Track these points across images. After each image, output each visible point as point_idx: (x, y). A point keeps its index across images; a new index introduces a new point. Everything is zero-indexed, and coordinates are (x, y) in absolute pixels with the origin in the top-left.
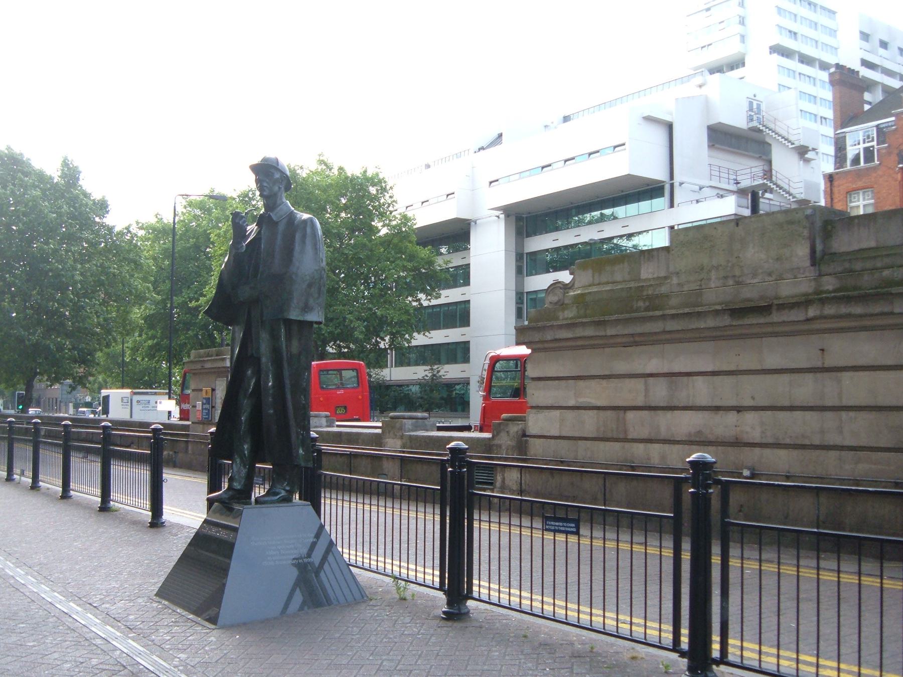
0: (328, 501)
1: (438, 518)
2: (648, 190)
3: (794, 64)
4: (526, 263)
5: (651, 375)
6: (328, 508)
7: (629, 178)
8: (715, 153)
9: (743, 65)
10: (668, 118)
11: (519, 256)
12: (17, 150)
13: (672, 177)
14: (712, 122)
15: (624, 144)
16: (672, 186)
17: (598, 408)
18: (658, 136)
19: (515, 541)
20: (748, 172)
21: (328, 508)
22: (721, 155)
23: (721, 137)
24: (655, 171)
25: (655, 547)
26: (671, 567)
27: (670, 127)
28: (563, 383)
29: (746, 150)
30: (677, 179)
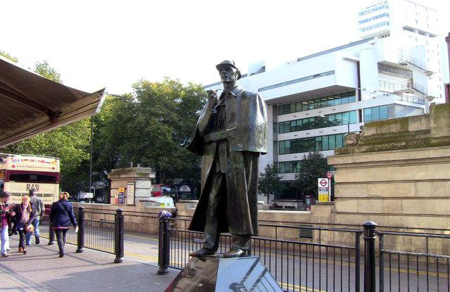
0: (173, 250)
1: (353, 265)
2: (347, 93)
3: (416, 35)
4: (278, 128)
5: (419, 181)
6: (173, 253)
7: (337, 87)
8: (380, 74)
9: (389, 35)
10: (357, 59)
11: (275, 124)
12: (173, 78)
13: (359, 86)
14: (381, 60)
15: (333, 72)
16: (360, 91)
17: (384, 198)
18: (353, 67)
19: (177, 260)
20: (399, 82)
21: (173, 253)
22: (385, 76)
23: (384, 67)
24: (350, 83)
25: (434, 272)
26: (354, 278)
27: (358, 63)
28: (359, 186)
29: (394, 73)
30: (363, 87)
